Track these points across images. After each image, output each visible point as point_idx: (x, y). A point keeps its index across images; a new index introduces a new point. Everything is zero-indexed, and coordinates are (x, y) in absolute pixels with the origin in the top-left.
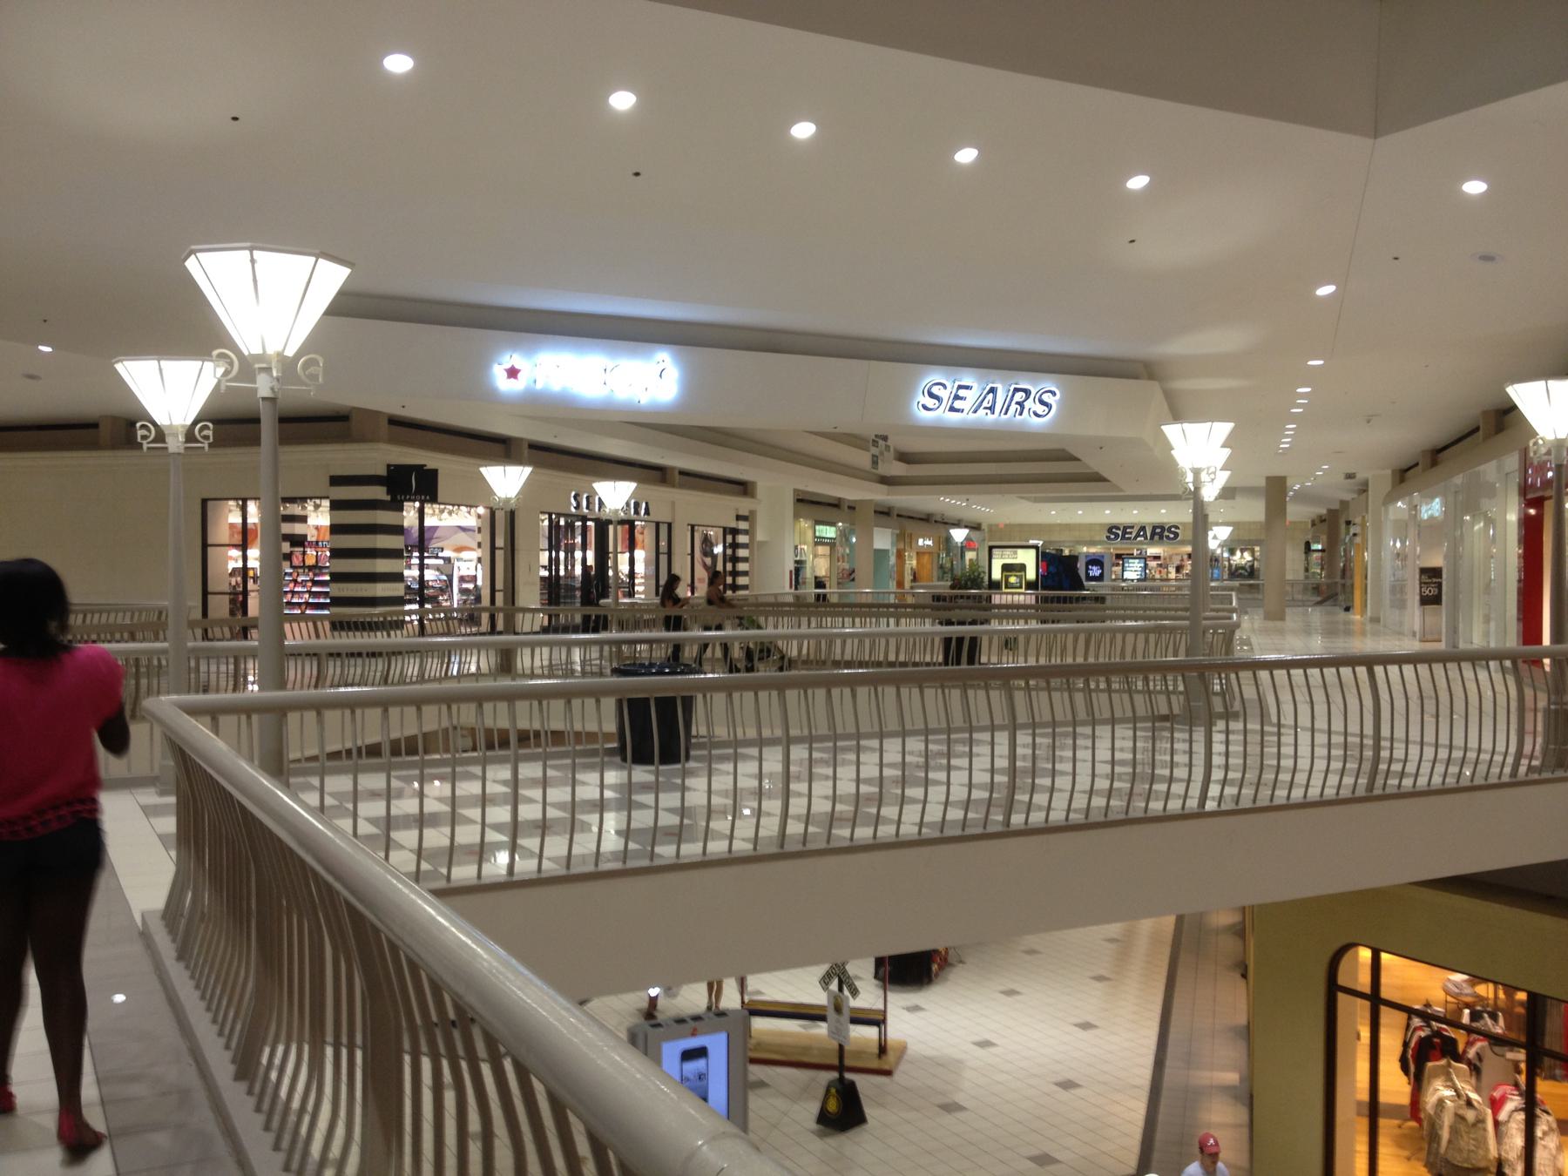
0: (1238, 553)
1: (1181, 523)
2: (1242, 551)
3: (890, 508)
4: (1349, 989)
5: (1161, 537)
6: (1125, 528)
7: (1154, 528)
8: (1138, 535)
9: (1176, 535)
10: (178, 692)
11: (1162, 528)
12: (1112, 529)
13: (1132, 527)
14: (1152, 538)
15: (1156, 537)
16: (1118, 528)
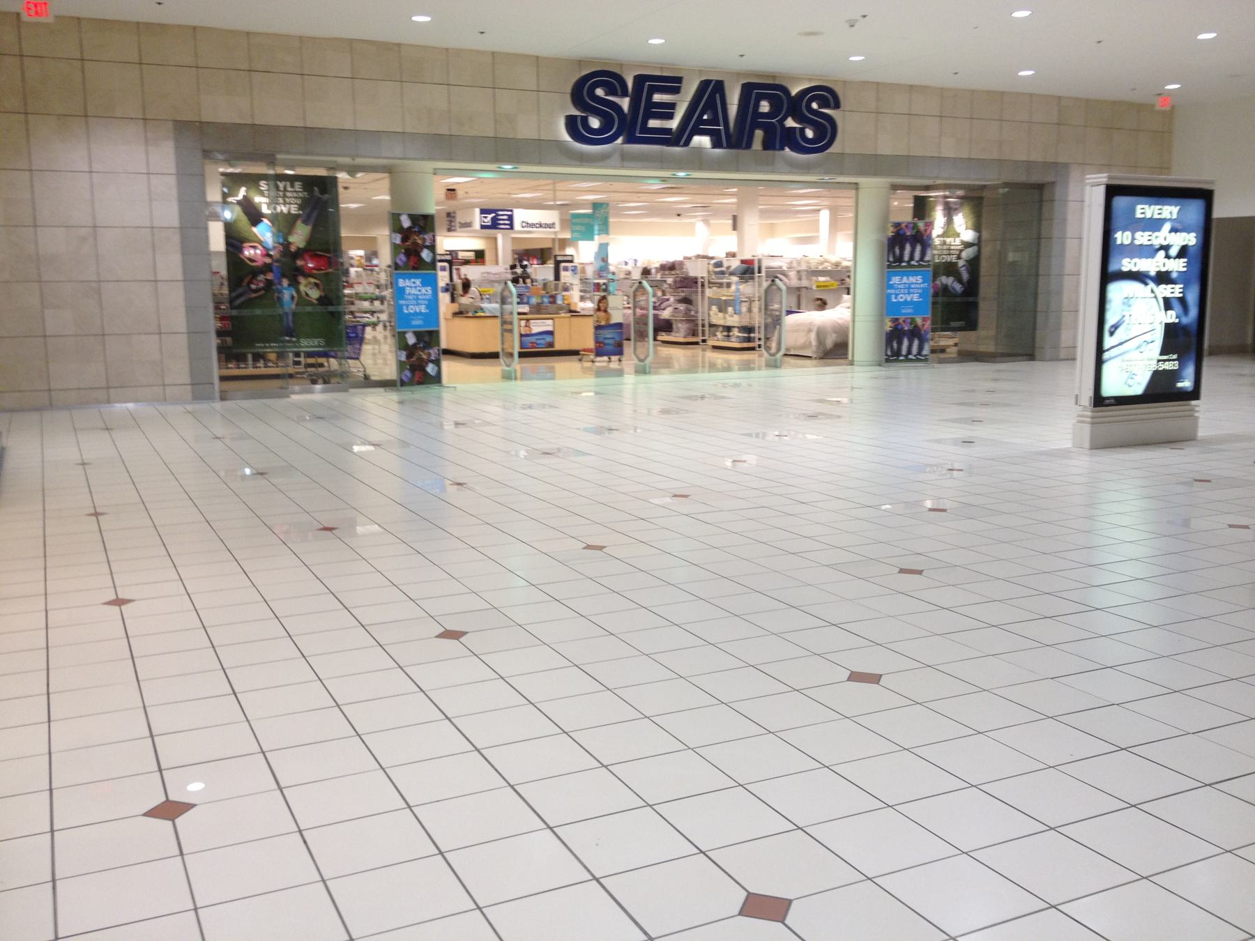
13: (672, 84)
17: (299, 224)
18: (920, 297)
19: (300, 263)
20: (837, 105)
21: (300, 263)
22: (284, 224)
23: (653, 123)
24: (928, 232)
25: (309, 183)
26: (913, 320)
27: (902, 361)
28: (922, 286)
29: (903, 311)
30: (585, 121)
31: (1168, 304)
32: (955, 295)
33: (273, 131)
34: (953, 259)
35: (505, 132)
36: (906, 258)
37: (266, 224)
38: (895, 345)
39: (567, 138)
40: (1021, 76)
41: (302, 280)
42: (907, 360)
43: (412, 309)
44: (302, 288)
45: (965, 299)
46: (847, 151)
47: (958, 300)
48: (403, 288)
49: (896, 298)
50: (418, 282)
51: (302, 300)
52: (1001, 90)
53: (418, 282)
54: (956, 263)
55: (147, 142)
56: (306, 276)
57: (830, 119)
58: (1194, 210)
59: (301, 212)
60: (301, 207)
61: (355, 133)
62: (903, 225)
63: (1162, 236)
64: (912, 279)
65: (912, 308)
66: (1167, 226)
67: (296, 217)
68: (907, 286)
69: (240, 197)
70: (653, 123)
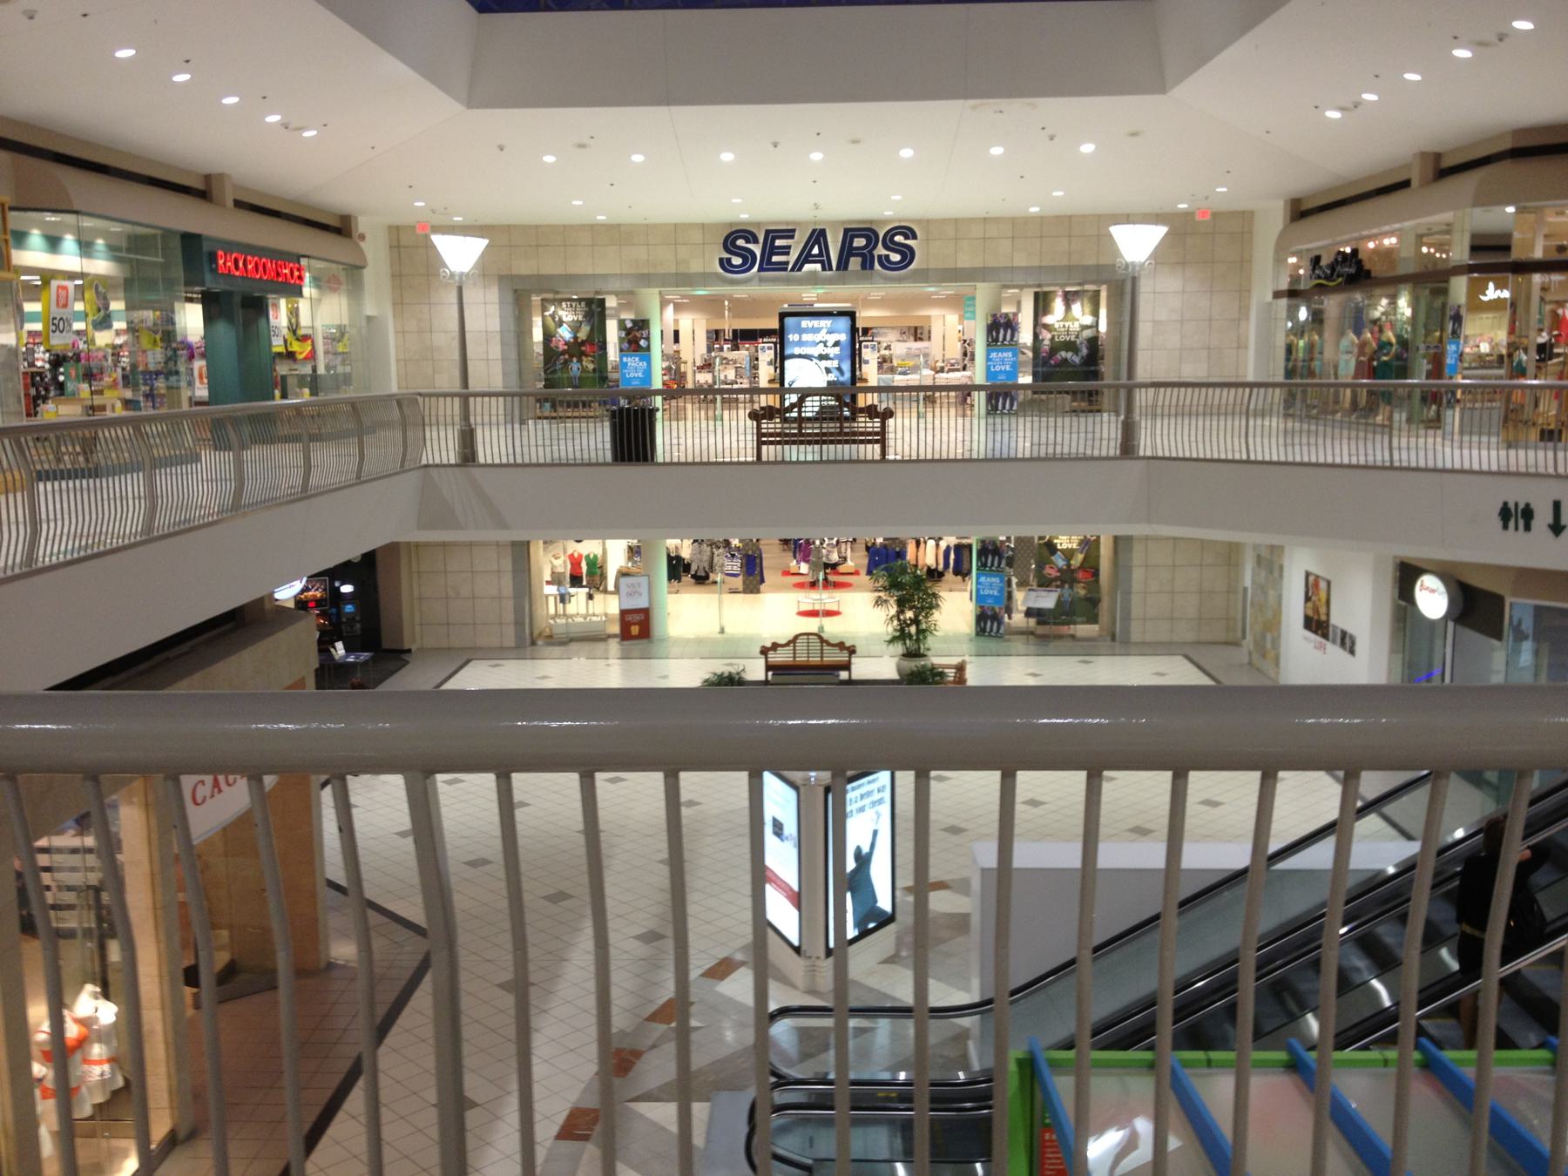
0: (1058, 305)
1: (919, 221)
2: (1069, 299)
3: (208, 178)
4: (998, 923)
5: (867, 264)
6: (771, 235)
7: (849, 234)
8: (805, 258)
9: (908, 255)
10: (1369, 378)
11: (869, 233)
12: (735, 239)
13: (789, 234)
14: (843, 265)
15: (855, 263)
16: (885, 263)
19: (583, 348)
20: (721, 260)
21: (583, 348)
22: (575, 327)
23: (775, 259)
25: (589, 302)
30: (729, 260)
31: (828, 371)
32: (1074, 366)
33: (549, 278)
34: (1073, 339)
35: (682, 269)
36: (1001, 339)
39: (721, 271)
41: (584, 358)
43: (632, 375)
44: (584, 363)
45: (1085, 369)
46: (931, 266)
47: (1080, 369)
48: (627, 363)
50: (637, 359)
51: (584, 370)
52: (1069, 213)
53: (637, 359)
54: (1075, 342)
55: (485, 288)
56: (587, 356)
57: (910, 248)
58: (844, 323)
60: (584, 317)
61: (594, 276)
63: (822, 336)
64: (1005, 354)
66: (825, 331)
67: (581, 322)
69: (551, 312)
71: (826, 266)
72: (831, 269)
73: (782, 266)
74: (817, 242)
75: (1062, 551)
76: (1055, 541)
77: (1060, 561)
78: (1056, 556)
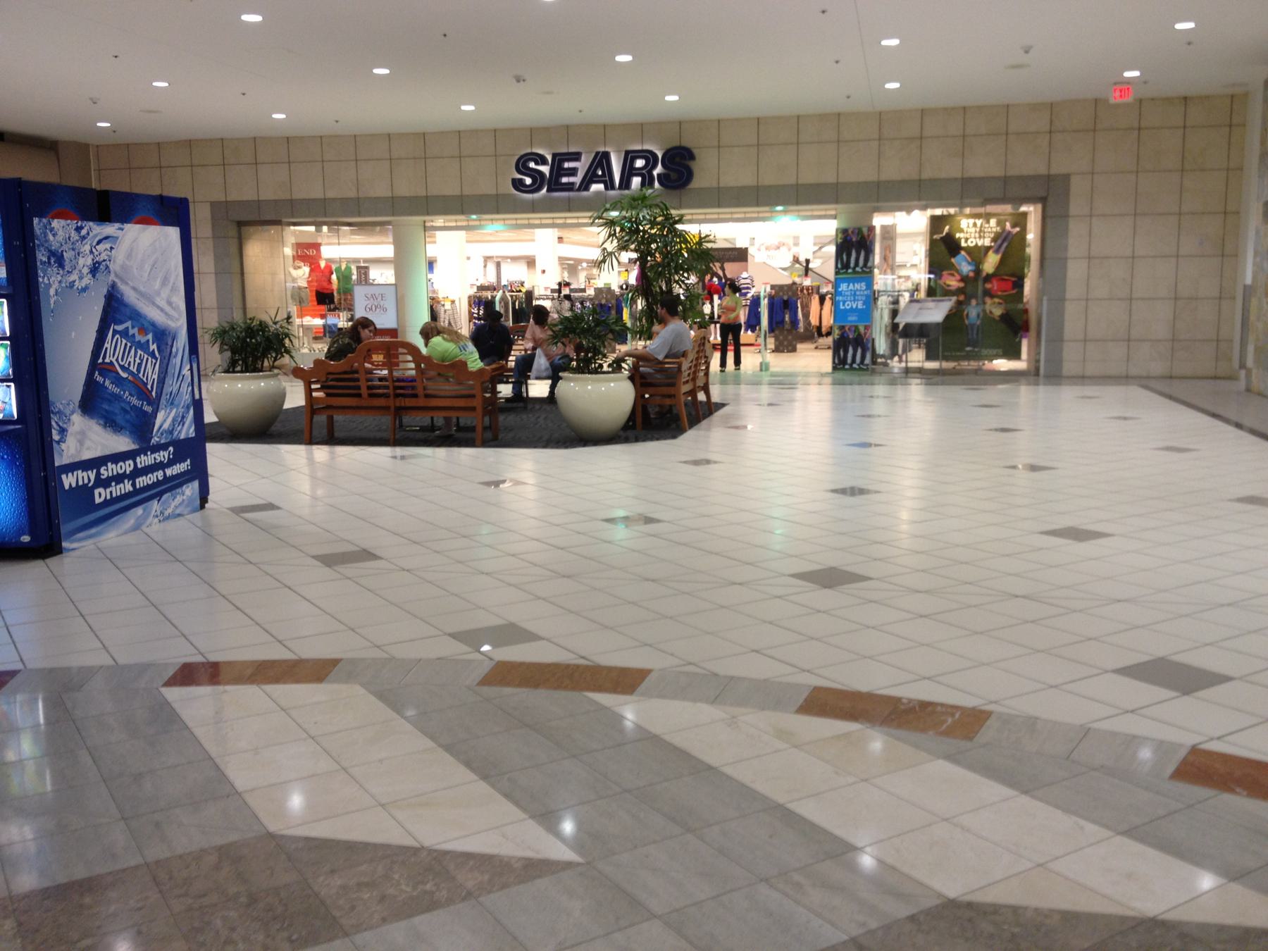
17: (991, 253)
18: (863, 304)
23: (565, 180)
24: (871, 237)
26: (856, 327)
27: (847, 369)
28: (866, 293)
29: (850, 319)
37: (964, 256)
38: (842, 353)
40: (889, 90)
42: (852, 368)
44: (988, 307)
49: (844, 305)
56: (992, 296)
59: (993, 244)
62: (850, 232)
64: (857, 286)
65: (856, 316)
68: (853, 293)
70: (565, 180)
71: (609, 185)
72: (613, 188)
73: (569, 187)
74: (600, 165)
75: (969, 251)
76: (958, 235)
77: (964, 265)
78: (959, 258)
